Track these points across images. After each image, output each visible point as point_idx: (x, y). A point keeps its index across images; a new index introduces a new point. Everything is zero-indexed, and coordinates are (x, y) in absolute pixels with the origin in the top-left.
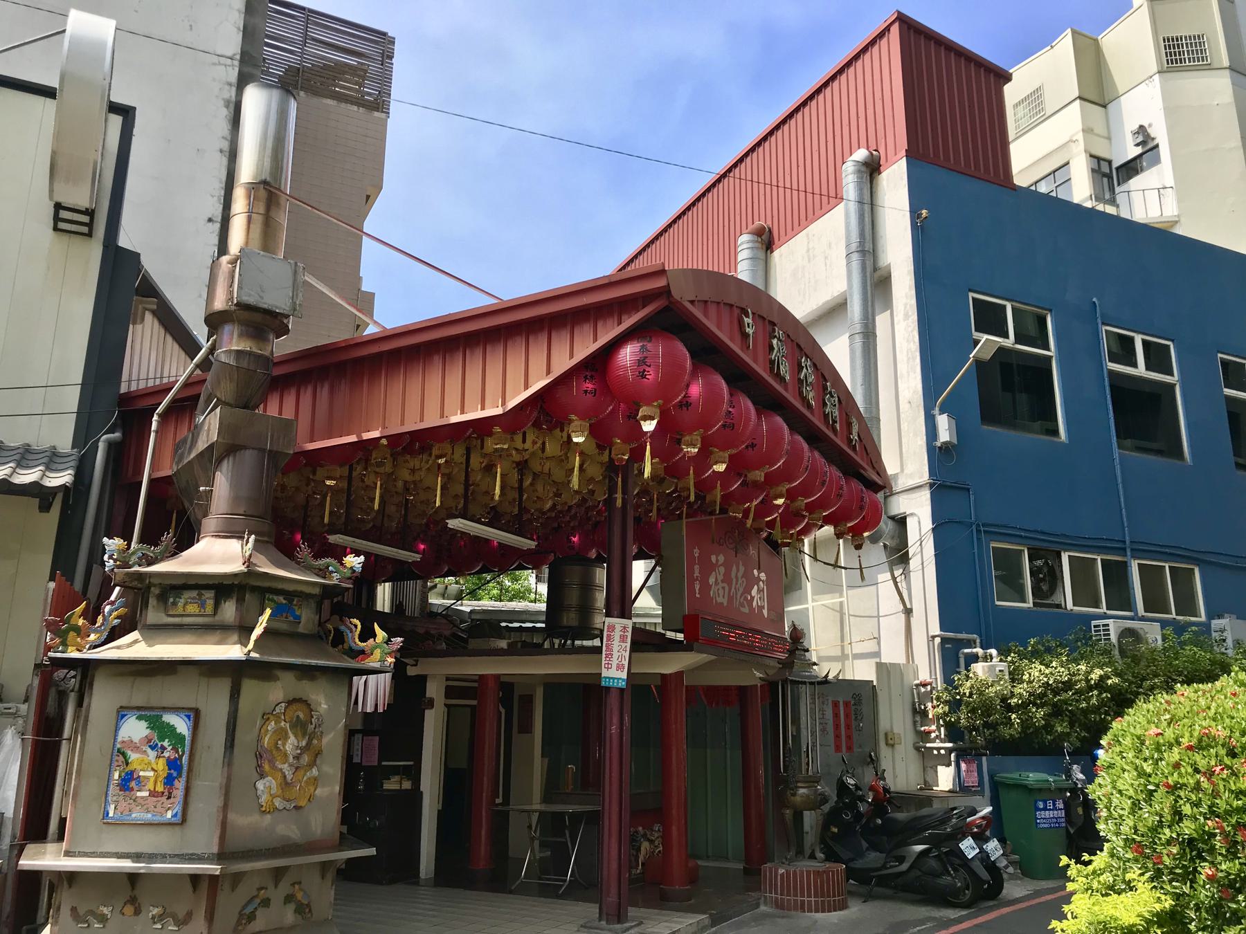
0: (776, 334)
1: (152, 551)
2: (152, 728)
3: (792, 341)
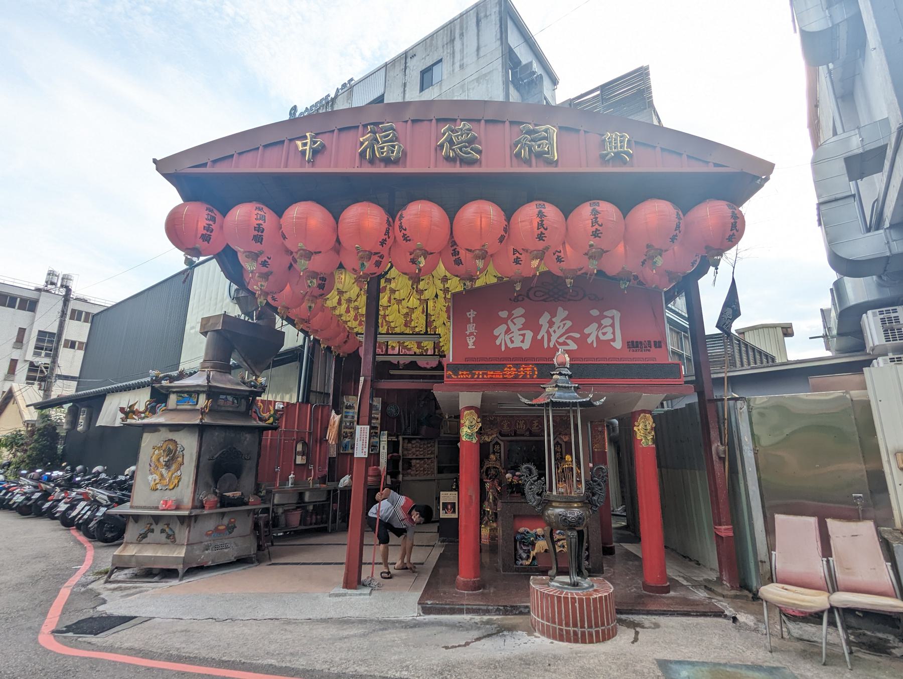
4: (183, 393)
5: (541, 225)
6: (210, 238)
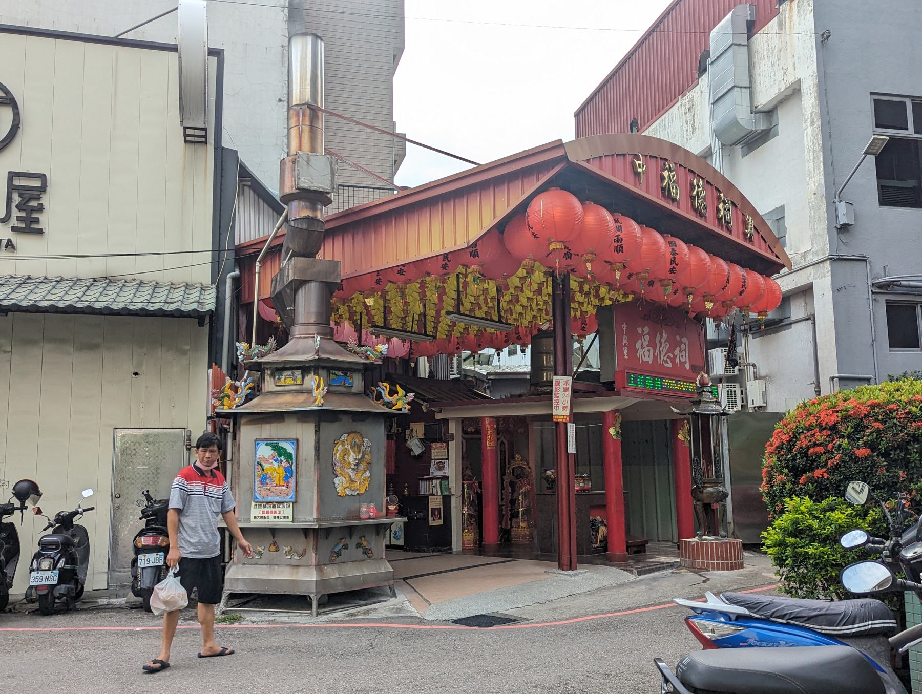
0: (667, 166)
1: (263, 349)
2: (274, 450)
3: (685, 168)
4: (337, 370)
5: (673, 261)
6: (622, 248)
